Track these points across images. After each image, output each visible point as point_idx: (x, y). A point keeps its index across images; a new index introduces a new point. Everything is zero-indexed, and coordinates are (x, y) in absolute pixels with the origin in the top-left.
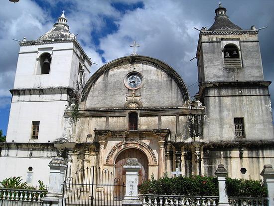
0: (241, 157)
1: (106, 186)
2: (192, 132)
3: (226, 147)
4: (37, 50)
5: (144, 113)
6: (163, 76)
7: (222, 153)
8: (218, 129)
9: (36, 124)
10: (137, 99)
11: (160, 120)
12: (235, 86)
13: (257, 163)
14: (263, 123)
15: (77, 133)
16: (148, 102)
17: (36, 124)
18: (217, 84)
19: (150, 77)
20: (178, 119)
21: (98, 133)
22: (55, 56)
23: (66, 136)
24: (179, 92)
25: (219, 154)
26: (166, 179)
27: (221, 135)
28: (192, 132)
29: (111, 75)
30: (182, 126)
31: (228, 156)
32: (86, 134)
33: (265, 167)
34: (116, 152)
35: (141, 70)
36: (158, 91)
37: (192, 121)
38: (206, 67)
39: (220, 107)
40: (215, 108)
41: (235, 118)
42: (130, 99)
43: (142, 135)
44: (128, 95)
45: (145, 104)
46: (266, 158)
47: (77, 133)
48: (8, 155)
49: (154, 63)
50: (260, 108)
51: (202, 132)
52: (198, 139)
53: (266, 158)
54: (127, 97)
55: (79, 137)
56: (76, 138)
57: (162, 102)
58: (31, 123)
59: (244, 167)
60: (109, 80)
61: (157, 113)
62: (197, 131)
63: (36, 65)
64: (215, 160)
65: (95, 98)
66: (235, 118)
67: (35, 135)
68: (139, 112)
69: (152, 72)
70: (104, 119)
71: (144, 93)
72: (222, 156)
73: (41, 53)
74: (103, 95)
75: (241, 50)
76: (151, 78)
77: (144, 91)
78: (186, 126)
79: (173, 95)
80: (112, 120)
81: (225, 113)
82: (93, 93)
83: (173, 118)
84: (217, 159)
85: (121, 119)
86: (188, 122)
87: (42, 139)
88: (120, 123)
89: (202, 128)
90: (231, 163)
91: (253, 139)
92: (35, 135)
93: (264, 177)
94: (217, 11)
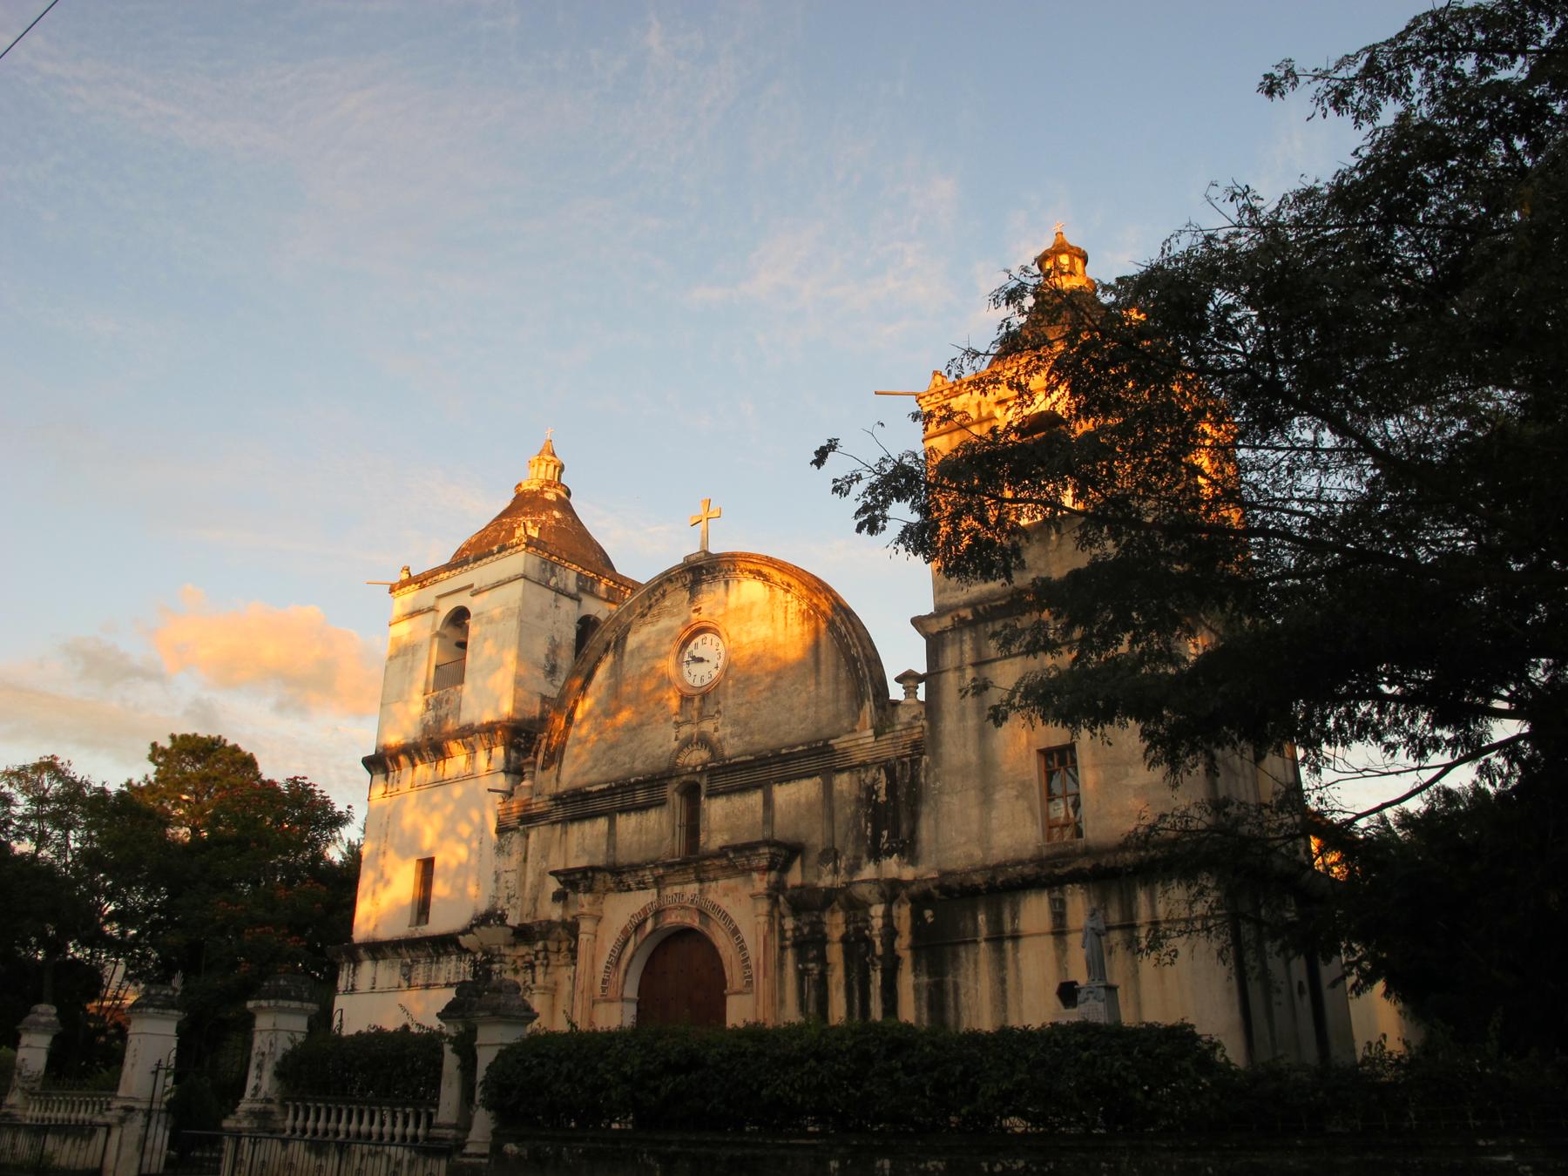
0: (1059, 931)
2: (876, 836)
3: (1000, 887)
4: (431, 603)
5: (721, 783)
6: (789, 616)
7: (981, 918)
8: (974, 813)
10: (707, 726)
11: (768, 803)
15: (528, 886)
16: (740, 736)
19: (749, 633)
20: (828, 788)
21: (573, 881)
22: (1053, 1001)
24: (843, 674)
25: (970, 925)
27: (984, 838)
28: (876, 836)
29: (632, 652)
30: (845, 812)
31: (1008, 928)
37: (876, 793)
41: (1040, 752)
42: (686, 730)
45: (733, 747)
51: (913, 832)
52: (893, 867)
54: (678, 725)
55: (535, 900)
56: (528, 907)
59: (1071, 978)
61: (760, 775)
62: (894, 834)
64: (956, 956)
66: (1040, 752)
68: (704, 783)
69: (755, 612)
70: (602, 824)
71: (730, 702)
72: (984, 930)
73: (446, 607)
76: (753, 637)
78: (856, 816)
79: (823, 690)
80: (627, 824)
83: (807, 789)
84: (962, 948)
85: (653, 816)
86: (863, 795)
87: (439, 923)
88: (647, 831)
89: (915, 817)
90: (1016, 961)
93: (801, 663)
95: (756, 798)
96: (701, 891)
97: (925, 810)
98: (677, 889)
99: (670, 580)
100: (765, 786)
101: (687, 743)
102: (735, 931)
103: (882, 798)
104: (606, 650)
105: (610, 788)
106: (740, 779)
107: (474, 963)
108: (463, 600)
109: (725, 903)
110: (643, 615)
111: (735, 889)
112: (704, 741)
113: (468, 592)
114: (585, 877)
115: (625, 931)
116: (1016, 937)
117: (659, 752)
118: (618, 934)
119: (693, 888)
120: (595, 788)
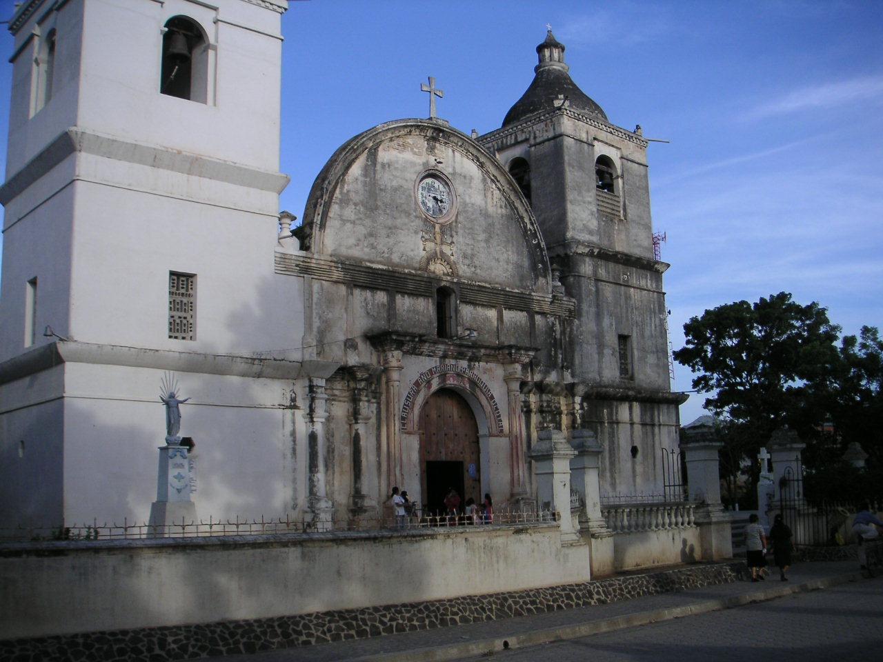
1: (672, 488)
9: (182, 282)
12: (620, 263)
13: (297, 431)
14: (657, 351)
17: (182, 282)
18: (596, 251)
36: (487, 241)
39: (598, 306)
40: (590, 306)
43: (471, 350)
46: (664, 425)
47: (315, 329)
50: (653, 321)
53: (664, 425)
57: (495, 272)
58: (166, 277)
60: (378, 176)
65: (349, 225)
67: (181, 325)
74: (368, 222)
75: (622, 177)
77: (461, 232)
81: (606, 322)
82: (342, 208)
92: (181, 325)
94: (540, 49)
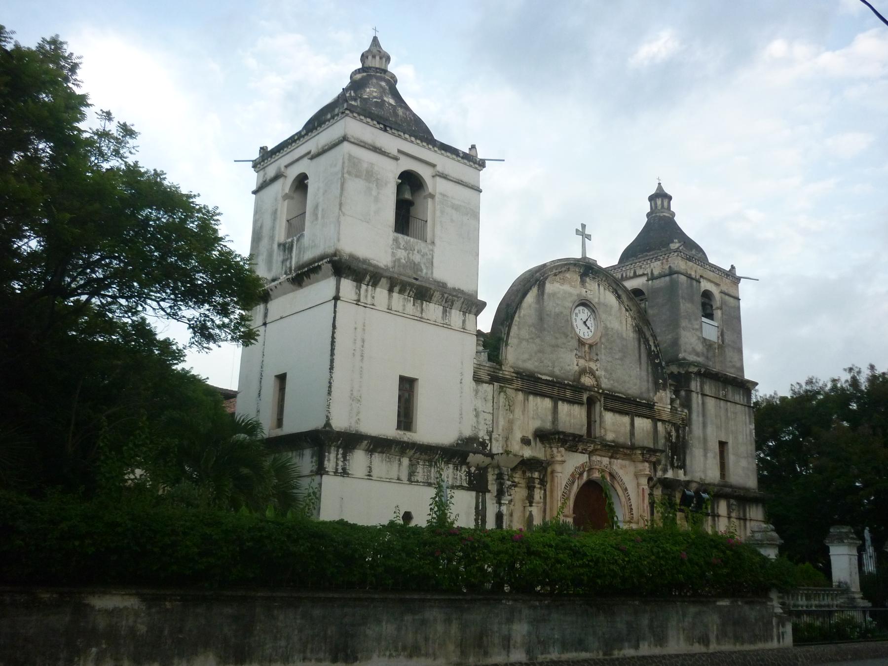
4: (395, 152)
9: (407, 385)
10: (593, 365)
15: (500, 427)
17: (407, 385)
23: (480, 436)
26: (504, 537)
32: (518, 435)
33: (753, 532)
34: (575, 489)
35: (597, 300)
36: (621, 359)
38: (684, 329)
41: (276, 376)
44: (579, 354)
48: (344, 469)
49: (617, 293)
61: (626, 407)
63: (311, 183)
66: (416, 380)
74: (538, 341)
91: (418, 423)
95: (626, 420)
96: (610, 463)
97: (688, 452)
98: (599, 458)
99: (575, 265)
100: (632, 415)
101: (583, 372)
102: (626, 489)
103: (674, 440)
104: (534, 284)
105: (552, 381)
106: (618, 405)
107: (469, 473)
108: (424, 172)
109: (621, 473)
110: (555, 275)
111: (625, 466)
112: (592, 373)
113: (306, 160)
114: (574, 440)
115: (573, 475)
116: (719, 516)
117: (568, 368)
118: (568, 476)
119: (606, 460)
120: (544, 377)
